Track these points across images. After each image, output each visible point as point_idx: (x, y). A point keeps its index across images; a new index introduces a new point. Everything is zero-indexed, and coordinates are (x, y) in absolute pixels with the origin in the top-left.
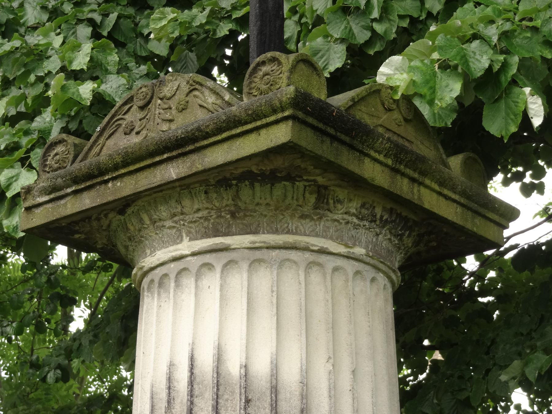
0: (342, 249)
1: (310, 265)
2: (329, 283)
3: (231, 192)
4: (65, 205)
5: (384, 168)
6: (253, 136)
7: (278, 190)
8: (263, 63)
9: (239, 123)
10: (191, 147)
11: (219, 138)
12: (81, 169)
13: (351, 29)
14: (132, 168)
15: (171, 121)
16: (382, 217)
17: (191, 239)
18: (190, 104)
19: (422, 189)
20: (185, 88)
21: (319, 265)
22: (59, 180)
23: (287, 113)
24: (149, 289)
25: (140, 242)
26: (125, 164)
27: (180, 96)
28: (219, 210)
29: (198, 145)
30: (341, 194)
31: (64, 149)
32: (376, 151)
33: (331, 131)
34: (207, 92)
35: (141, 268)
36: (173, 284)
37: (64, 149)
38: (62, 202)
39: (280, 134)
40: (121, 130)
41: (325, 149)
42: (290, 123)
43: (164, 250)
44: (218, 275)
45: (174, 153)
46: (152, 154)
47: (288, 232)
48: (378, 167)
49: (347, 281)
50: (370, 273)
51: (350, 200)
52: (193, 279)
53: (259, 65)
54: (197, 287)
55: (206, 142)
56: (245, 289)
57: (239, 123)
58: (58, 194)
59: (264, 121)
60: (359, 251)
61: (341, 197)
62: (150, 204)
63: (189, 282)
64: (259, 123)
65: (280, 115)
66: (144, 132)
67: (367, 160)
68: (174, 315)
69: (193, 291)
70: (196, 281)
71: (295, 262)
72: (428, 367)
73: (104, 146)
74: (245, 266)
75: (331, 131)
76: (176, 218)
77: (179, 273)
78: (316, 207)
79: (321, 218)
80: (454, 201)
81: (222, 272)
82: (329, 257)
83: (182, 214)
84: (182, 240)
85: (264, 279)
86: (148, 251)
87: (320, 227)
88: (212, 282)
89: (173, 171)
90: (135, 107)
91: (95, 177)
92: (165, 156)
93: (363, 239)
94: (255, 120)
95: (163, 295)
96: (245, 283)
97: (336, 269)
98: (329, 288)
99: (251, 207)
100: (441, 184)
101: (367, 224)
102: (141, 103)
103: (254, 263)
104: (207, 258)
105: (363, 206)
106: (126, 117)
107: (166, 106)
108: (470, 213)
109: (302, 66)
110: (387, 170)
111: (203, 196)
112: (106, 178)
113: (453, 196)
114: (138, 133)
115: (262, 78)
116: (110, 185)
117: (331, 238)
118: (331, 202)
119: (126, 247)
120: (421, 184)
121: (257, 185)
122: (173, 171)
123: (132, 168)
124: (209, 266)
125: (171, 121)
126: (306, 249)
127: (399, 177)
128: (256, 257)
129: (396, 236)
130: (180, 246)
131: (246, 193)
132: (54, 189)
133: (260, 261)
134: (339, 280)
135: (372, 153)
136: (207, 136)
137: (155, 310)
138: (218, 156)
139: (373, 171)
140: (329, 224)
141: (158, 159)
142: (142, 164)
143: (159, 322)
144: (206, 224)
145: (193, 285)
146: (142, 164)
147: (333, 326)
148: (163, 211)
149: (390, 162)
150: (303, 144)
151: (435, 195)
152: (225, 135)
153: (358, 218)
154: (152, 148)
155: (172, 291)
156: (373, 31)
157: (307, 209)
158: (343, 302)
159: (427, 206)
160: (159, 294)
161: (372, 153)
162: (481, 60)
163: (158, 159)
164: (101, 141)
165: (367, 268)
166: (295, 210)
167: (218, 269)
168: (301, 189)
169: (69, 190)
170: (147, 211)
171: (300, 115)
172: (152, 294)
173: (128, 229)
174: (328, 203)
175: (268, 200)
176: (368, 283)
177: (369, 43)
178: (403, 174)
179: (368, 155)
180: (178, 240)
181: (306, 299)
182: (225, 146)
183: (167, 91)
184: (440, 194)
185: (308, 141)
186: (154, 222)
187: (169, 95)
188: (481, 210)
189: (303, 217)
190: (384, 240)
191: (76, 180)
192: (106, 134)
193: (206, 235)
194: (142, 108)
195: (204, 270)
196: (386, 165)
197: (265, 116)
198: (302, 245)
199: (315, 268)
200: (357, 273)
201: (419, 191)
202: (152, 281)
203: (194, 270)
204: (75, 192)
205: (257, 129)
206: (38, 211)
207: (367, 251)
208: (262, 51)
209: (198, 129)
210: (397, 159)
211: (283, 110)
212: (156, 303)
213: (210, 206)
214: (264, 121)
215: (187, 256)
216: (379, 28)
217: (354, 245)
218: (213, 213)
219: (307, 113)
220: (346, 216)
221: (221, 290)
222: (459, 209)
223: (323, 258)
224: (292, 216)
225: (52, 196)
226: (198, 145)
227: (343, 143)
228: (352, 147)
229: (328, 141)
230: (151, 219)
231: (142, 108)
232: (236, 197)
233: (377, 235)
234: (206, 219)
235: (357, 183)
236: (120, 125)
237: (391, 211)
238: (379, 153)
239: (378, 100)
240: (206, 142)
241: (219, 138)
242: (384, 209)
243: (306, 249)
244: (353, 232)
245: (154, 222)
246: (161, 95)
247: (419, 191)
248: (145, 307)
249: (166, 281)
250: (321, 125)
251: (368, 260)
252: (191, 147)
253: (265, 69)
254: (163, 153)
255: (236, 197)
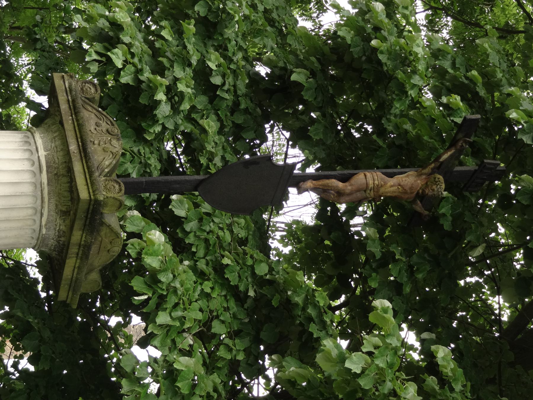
0: (44, 223)
1: (35, 209)
2: (30, 217)
3: (65, 173)
4: (63, 96)
5: (80, 240)
6: (85, 183)
7: (67, 194)
8: (120, 186)
9: (91, 176)
10: (83, 155)
11: (85, 168)
12: (78, 103)
13: (191, 221)
14: (77, 128)
15: (99, 144)
16: (61, 241)
17: (45, 155)
18: (106, 153)
19: (75, 259)
20: (114, 151)
21: (36, 213)
22: (74, 93)
23: (92, 197)
24: (25, 136)
25: (47, 131)
26: (79, 125)
27: (111, 149)
28: (58, 168)
29: (83, 158)
30: (68, 222)
31: (93, 92)
32: (86, 236)
33: (89, 216)
34: (110, 161)
35: (35, 132)
36: (25, 148)
37: (93, 92)
38: (65, 94)
39: (84, 194)
40: (99, 121)
41: (81, 214)
42: (88, 198)
43: (42, 143)
44: (29, 169)
45: (81, 148)
46: (81, 138)
47: (49, 199)
48: (79, 237)
49: (30, 226)
50: (35, 236)
51: (65, 226)
52: (27, 157)
53: (119, 184)
54: (24, 159)
55: (84, 162)
56: (22, 181)
57: (91, 176)
58: (68, 92)
59: (90, 187)
60: (44, 231)
61: (66, 222)
62: (62, 136)
63: (27, 155)
64: (89, 185)
65: (92, 194)
66: (95, 132)
67: (81, 232)
68: (11, 150)
69: (22, 158)
70: (26, 159)
71: (36, 203)
72: (98, 300)
73: (92, 112)
74: (33, 180)
75: (89, 216)
76: (55, 148)
77: (30, 151)
78: (61, 211)
79: (57, 213)
80: (73, 274)
81: (30, 170)
82: (39, 217)
83: (57, 151)
84: (45, 151)
85: (28, 189)
86: (42, 135)
87: (52, 213)
88: (26, 166)
89: (73, 147)
90: (108, 126)
91: (74, 110)
92: (80, 144)
93: (50, 233)
94: (91, 183)
95: (21, 143)
96: (25, 181)
97: (34, 220)
98: (26, 218)
99: (60, 182)
100: (79, 268)
101: (57, 234)
102: (110, 130)
103: (34, 184)
104: (37, 164)
105: (64, 232)
106: (105, 123)
107: (106, 142)
108: (69, 282)
109: (118, 203)
110: (79, 241)
111: (64, 161)
112: (73, 116)
113: (75, 274)
114: (95, 129)
115: (113, 185)
116: (70, 118)
117: (48, 218)
118: (64, 217)
119: (46, 124)
120: (77, 257)
121: (69, 185)
122: (73, 147)
123: (77, 128)
124: (33, 164)
125: (99, 144)
126: (42, 207)
127: (77, 247)
128: (37, 185)
129: (54, 248)
130: (43, 150)
131: (65, 180)
132: (71, 90)
133: (36, 187)
134: (30, 222)
135: (84, 235)
136: (87, 162)
137: (14, 140)
138: (78, 167)
139: (77, 236)
140: (55, 217)
141: (79, 140)
142: (78, 133)
143: (8, 142)
144: (52, 162)
145: (24, 158)
146: (78, 133)
147: (7, 220)
148: (58, 143)
149: (83, 243)
150: (80, 204)
151: (73, 265)
152: (86, 170)
153: (59, 229)
154: (84, 137)
155: (22, 148)
156: (190, 233)
157: (60, 207)
158: (19, 224)
159: (67, 261)
160: (22, 141)
161: (84, 235)
162: (163, 278)
163: (79, 140)
164: (94, 111)
165: (37, 235)
166: (59, 202)
167: (32, 169)
168: (68, 204)
169: (70, 98)
170: (59, 135)
171: (92, 203)
172: (21, 139)
173: (53, 125)
174: (63, 216)
175: (62, 190)
176: (30, 236)
177: (183, 230)
178: (79, 249)
179: (83, 233)
180: (46, 149)
181: (19, 208)
182: (82, 171)
183: (114, 142)
184: (75, 267)
185: (82, 207)
186: (54, 138)
187: (112, 143)
188: (72, 288)
189: (56, 205)
190: (52, 242)
191: (74, 101)
192: (97, 113)
193: (47, 162)
194: (107, 131)
195: (32, 162)
196: (81, 241)
197: (92, 188)
198: (44, 205)
199: (34, 211)
200: (34, 231)
201: (73, 257)
202: (28, 138)
203: (32, 158)
204: (68, 101)
205: (87, 185)
206: (62, 82)
207: (44, 235)
208: (125, 183)
209: (90, 159)
210: (85, 246)
211: (94, 195)
212: (17, 140)
213: (60, 164)
214: (90, 187)
215: (38, 154)
216: (191, 235)
217: (46, 229)
218: (57, 165)
219: (94, 205)
220: (58, 224)
221: (22, 170)
222: (70, 277)
223: (39, 215)
224: (56, 201)
225: (68, 89)
226: (83, 158)
227: (86, 221)
228: (85, 225)
229: (85, 215)
230: (56, 136)
231: (107, 131)
232: (63, 176)
233: (53, 239)
234: (54, 162)
235: (71, 228)
236: (101, 120)
237: (64, 245)
238: (85, 238)
239: (114, 237)
240: (84, 162)
241: (85, 168)
242: (64, 242)
243: (42, 207)
244: (52, 228)
245: (54, 138)
246: (112, 140)
247: (73, 257)
248: (17, 135)
249: (28, 144)
250: (90, 211)
251: (41, 235)
252: (83, 155)
253: (117, 187)
254: (82, 143)
255: (63, 176)
